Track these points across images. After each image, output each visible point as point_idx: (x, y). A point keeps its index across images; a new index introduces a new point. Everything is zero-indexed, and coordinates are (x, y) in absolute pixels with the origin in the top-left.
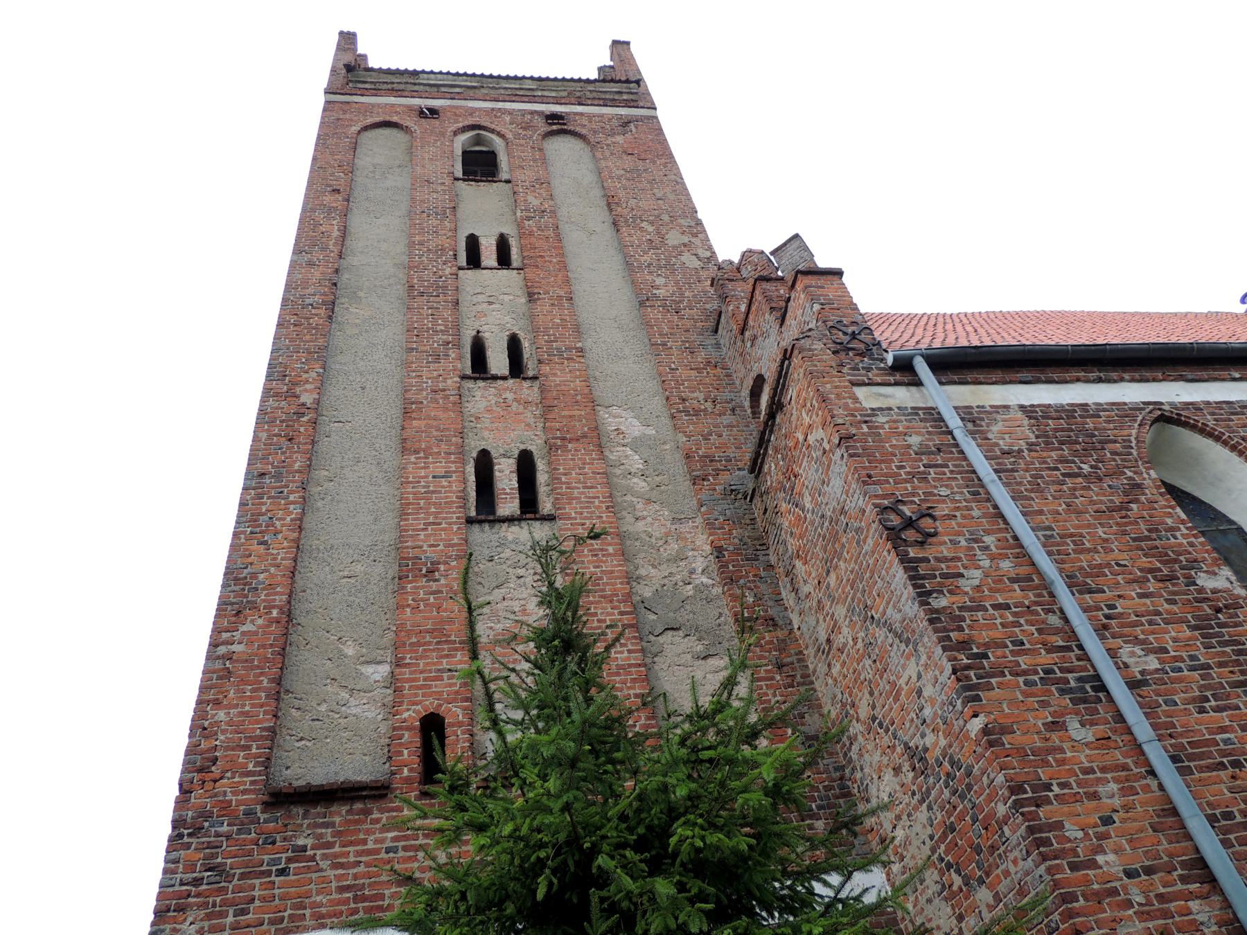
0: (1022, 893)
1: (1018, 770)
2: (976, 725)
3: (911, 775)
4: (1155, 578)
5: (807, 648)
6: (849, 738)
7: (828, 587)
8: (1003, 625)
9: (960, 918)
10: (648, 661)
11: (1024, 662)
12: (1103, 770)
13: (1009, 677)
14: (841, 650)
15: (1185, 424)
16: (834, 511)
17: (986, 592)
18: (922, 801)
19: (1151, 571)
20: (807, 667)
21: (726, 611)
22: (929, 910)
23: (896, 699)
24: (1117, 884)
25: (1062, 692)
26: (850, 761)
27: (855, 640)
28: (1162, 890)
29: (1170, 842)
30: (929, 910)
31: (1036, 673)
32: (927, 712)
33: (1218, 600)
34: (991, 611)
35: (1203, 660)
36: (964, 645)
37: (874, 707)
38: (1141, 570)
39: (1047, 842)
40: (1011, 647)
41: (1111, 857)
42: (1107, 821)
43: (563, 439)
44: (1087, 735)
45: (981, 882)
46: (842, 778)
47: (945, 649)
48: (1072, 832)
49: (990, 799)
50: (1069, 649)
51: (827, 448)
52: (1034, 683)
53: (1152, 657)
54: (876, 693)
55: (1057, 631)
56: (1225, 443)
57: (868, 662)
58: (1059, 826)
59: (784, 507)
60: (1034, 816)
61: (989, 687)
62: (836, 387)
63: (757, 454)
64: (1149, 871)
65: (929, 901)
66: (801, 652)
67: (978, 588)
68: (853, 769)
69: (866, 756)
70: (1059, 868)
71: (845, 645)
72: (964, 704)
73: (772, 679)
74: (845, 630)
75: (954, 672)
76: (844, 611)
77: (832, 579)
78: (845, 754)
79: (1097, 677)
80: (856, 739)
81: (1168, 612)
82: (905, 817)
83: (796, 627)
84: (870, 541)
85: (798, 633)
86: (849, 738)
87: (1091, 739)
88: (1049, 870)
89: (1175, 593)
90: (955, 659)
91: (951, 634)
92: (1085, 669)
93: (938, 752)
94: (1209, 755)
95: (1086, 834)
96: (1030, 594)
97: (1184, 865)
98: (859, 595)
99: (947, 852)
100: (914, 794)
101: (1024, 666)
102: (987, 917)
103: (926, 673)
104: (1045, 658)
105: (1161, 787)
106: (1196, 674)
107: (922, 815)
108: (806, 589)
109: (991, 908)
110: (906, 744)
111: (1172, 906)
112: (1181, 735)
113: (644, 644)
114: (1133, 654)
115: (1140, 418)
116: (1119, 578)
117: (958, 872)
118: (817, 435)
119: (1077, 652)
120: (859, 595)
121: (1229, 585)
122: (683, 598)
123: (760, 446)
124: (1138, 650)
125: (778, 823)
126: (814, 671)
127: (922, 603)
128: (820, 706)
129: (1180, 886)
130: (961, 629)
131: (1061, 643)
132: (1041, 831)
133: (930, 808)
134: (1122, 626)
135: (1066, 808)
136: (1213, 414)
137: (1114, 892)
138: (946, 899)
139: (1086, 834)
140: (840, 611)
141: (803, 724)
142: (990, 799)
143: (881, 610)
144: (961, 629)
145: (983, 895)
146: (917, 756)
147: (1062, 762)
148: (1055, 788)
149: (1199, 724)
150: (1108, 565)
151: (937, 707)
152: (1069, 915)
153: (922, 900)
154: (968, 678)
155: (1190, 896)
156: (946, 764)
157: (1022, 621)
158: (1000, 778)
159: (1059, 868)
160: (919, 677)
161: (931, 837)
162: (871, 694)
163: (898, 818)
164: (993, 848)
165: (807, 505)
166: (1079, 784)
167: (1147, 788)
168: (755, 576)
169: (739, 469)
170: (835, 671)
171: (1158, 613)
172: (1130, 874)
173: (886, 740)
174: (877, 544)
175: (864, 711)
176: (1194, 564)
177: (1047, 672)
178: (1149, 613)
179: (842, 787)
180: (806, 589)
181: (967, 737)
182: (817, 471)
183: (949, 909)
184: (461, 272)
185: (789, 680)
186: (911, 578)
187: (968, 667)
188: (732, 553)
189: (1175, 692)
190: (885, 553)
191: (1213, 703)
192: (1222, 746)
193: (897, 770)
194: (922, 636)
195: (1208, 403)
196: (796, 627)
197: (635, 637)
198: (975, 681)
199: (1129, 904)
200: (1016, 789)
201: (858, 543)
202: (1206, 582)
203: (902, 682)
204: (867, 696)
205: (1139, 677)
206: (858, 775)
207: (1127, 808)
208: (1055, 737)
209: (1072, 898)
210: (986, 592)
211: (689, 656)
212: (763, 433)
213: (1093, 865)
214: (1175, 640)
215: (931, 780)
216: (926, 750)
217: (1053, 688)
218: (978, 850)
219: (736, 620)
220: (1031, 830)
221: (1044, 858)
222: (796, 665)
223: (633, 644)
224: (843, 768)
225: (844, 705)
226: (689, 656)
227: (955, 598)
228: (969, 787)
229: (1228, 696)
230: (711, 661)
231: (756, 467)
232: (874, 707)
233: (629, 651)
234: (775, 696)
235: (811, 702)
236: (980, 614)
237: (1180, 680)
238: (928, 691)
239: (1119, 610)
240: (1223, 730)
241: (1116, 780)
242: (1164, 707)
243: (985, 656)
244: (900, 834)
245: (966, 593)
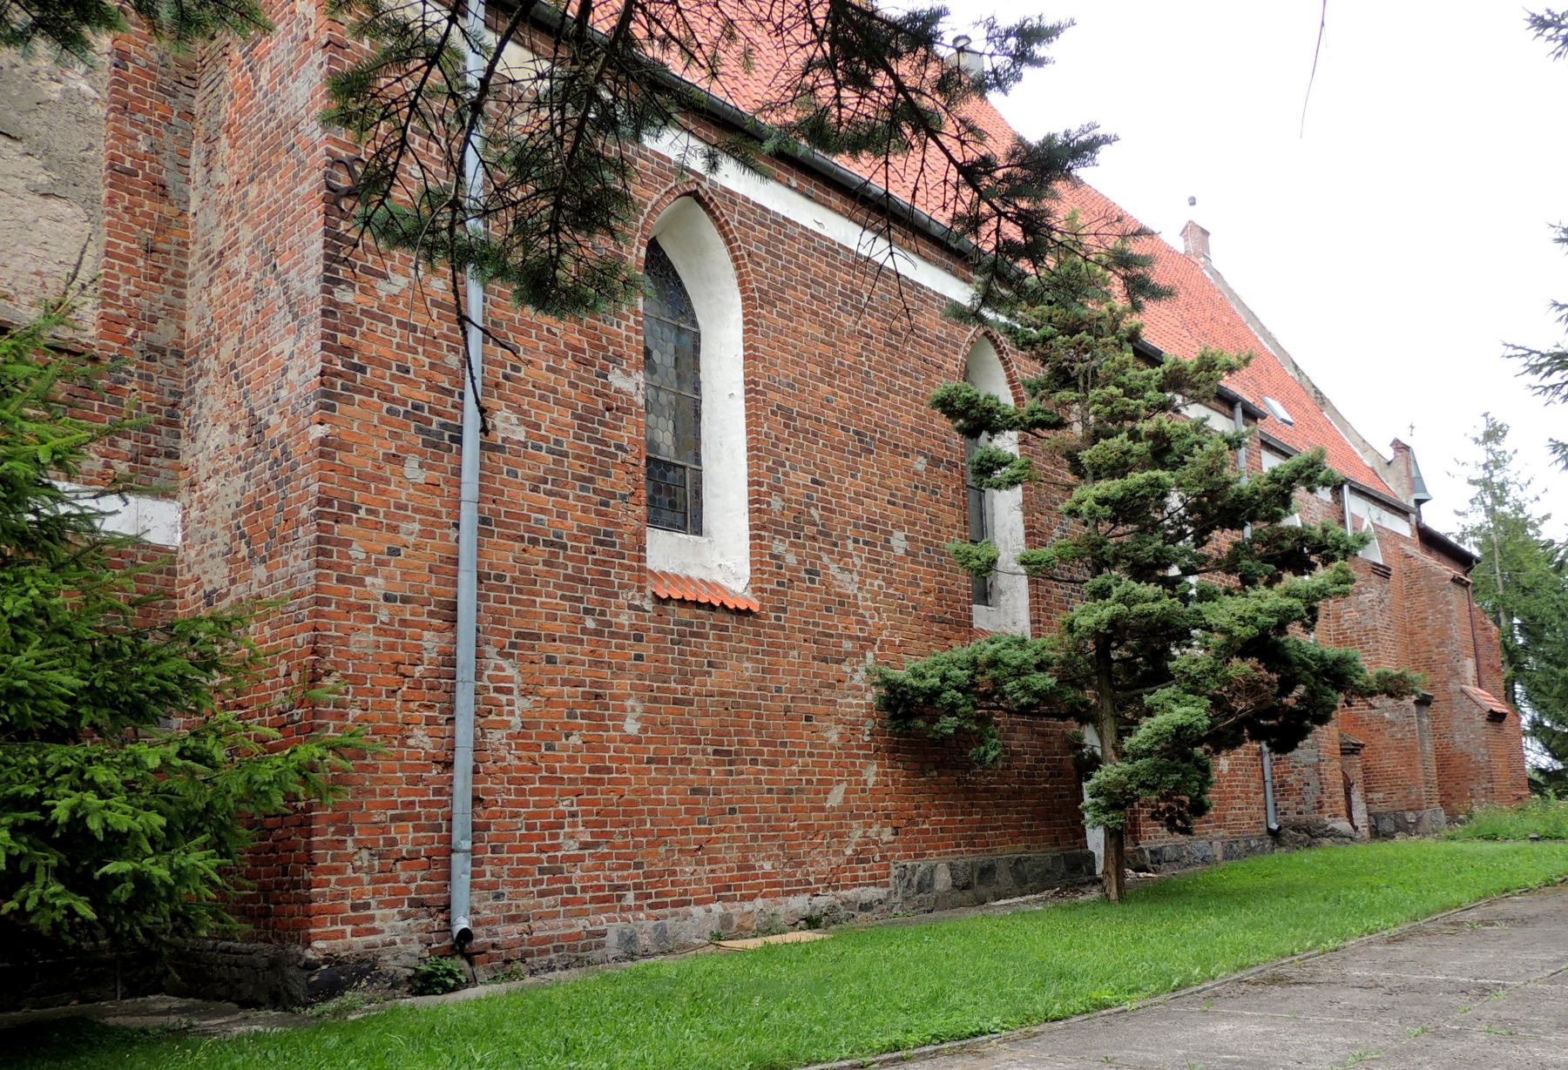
0: (290, 584)
1: (335, 484)
2: (318, 432)
3: (244, 440)
4: (574, 357)
5: (195, 243)
6: (201, 369)
7: (246, 195)
8: (399, 346)
9: (233, 582)
11: (399, 390)
13: (375, 399)
15: (711, 212)
16: (287, 117)
17: (401, 306)
18: (243, 469)
19: (575, 349)
20: (186, 265)
21: (101, 145)
22: (209, 564)
23: (262, 362)
24: (372, 603)
25: (419, 430)
26: (192, 392)
28: (408, 617)
29: (438, 584)
30: (209, 564)
31: (405, 404)
32: (283, 393)
33: (615, 400)
34: (394, 327)
35: (565, 448)
36: (346, 351)
37: (237, 356)
38: (566, 345)
39: (329, 554)
40: (394, 370)
41: (379, 581)
42: (394, 552)
44: (420, 476)
45: (263, 560)
46: (174, 405)
47: (324, 347)
48: (356, 551)
49: (299, 499)
50: (450, 393)
51: (312, 37)
52: (397, 413)
53: (522, 429)
54: (246, 343)
55: (450, 372)
56: (732, 250)
57: (251, 308)
58: (348, 544)
59: (236, 54)
60: (329, 529)
61: (350, 401)
64: (405, 600)
65: (213, 556)
66: (185, 244)
67: (394, 298)
69: (210, 398)
71: (236, 272)
74: (243, 258)
75: (322, 374)
76: (250, 237)
77: (253, 190)
78: (190, 383)
79: (460, 429)
80: (207, 374)
81: (564, 394)
82: (222, 474)
83: (192, 210)
84: (306, 184)
85: (191, 219)
86: (201, 369)
88: (317, 576)
89: (581, 379)
90: (330, 362)
91: (339, 335)
92: (454, 417)
93: (276, 435)
94: (516, 527)
95: (368, 558)
96: (445, 325)
97: (438, 603)
98: (272, 232)
99: (246, 523)
100: (239, 458)
101: (396, 394)
102: (255, 590)
103: (298, 356)
104: (422, 394)
105: (457, 540)
106: (551, 457)
109: (261, 584)
110: (252, 410)
111: (409, 631)
112: (504, 504)
115: (672, 185)
116: (541, 344)
117: (248, 544)
119: (456, 399)
120: (272, 232)
121: (633, 390)
122: (41, 98)
124: (514, 418)
126: (192, 275)
127: (326, 290)
128: (183, 317)
129: (425, 618)
130: (352, 333)
132: (328, 543)
133: (247, 479)
134: (514, 390)
135: (362, 531)
136: (742, 214)
137: (366, 608)
138: (228, 561)
140: (247, 234)
141: (151, 330)
142: (299, 499)
143: (286, 265)
144: (352, 333)
145: (260, 572)
146: (257, 428)
147: (380, 492)
149: (523, 499)
150: (539, 327)
151: (293, 395)
152: (317, 614)
153: (207, 553)
154: (333, 385)
155: (429, 627)
156: (278, 449)
157: (420, 349)
158: (315, 488)
159: (327, 577)
161: (238, 505)
162: (241, 341)
163: (216, 471)
165: (263, 82)
166: (386, 515)
167: (445, 537)
168: (163, 117)
170: (216, 290)
171: (554, 391)
172: (387, 598)
174: (310, 196)
175: (226, 353)
176: (617, 359)
177: (415, 407)
178: (547, 388)
179: (171, 415)
180: (220, 177)
181: (305, 438)
182: (290, 52)
183: (226, 571)
185: (155, 272)
186: (327, 257)
187: (338, 375)
188: (139, 70)
189: (522, 466)
190: (315, 212)
191: (549, 486)
192: (532, 524)
193: (234, 428)
194: (310, 321)
195: (747, 200)
196: (192, 210)
198: (339, 390)
199: (373, 620)
200: (324, 501)
201: (295, 176)
202: (617, 379)
205: (500, 442)
207: (417, 547)
208: (388, 469)
210: (401, 306)
211: (22, 184)
213: (360, 582)
214: (553, 421)
215: (260, 456)
217: (413, 424)
219: (111, 166)
220: (319, 540)
221: (319, 565)
222: (172, 256)
224: (181, 395)
225: (209, 333)
226: (22, 184)
227: (363, 298)
228: (288, 480)
229: (565, 485)
230: (53, 204)
232: (237, 356)
235: (175, 313)
236: (381, 325)
237: (533, 457)
239: (522, 375)
240: (542, 511)
241: (422, 522)
242: (505, 476)
243: (362, 370)
244: (211, 486)
245: (379, 298)
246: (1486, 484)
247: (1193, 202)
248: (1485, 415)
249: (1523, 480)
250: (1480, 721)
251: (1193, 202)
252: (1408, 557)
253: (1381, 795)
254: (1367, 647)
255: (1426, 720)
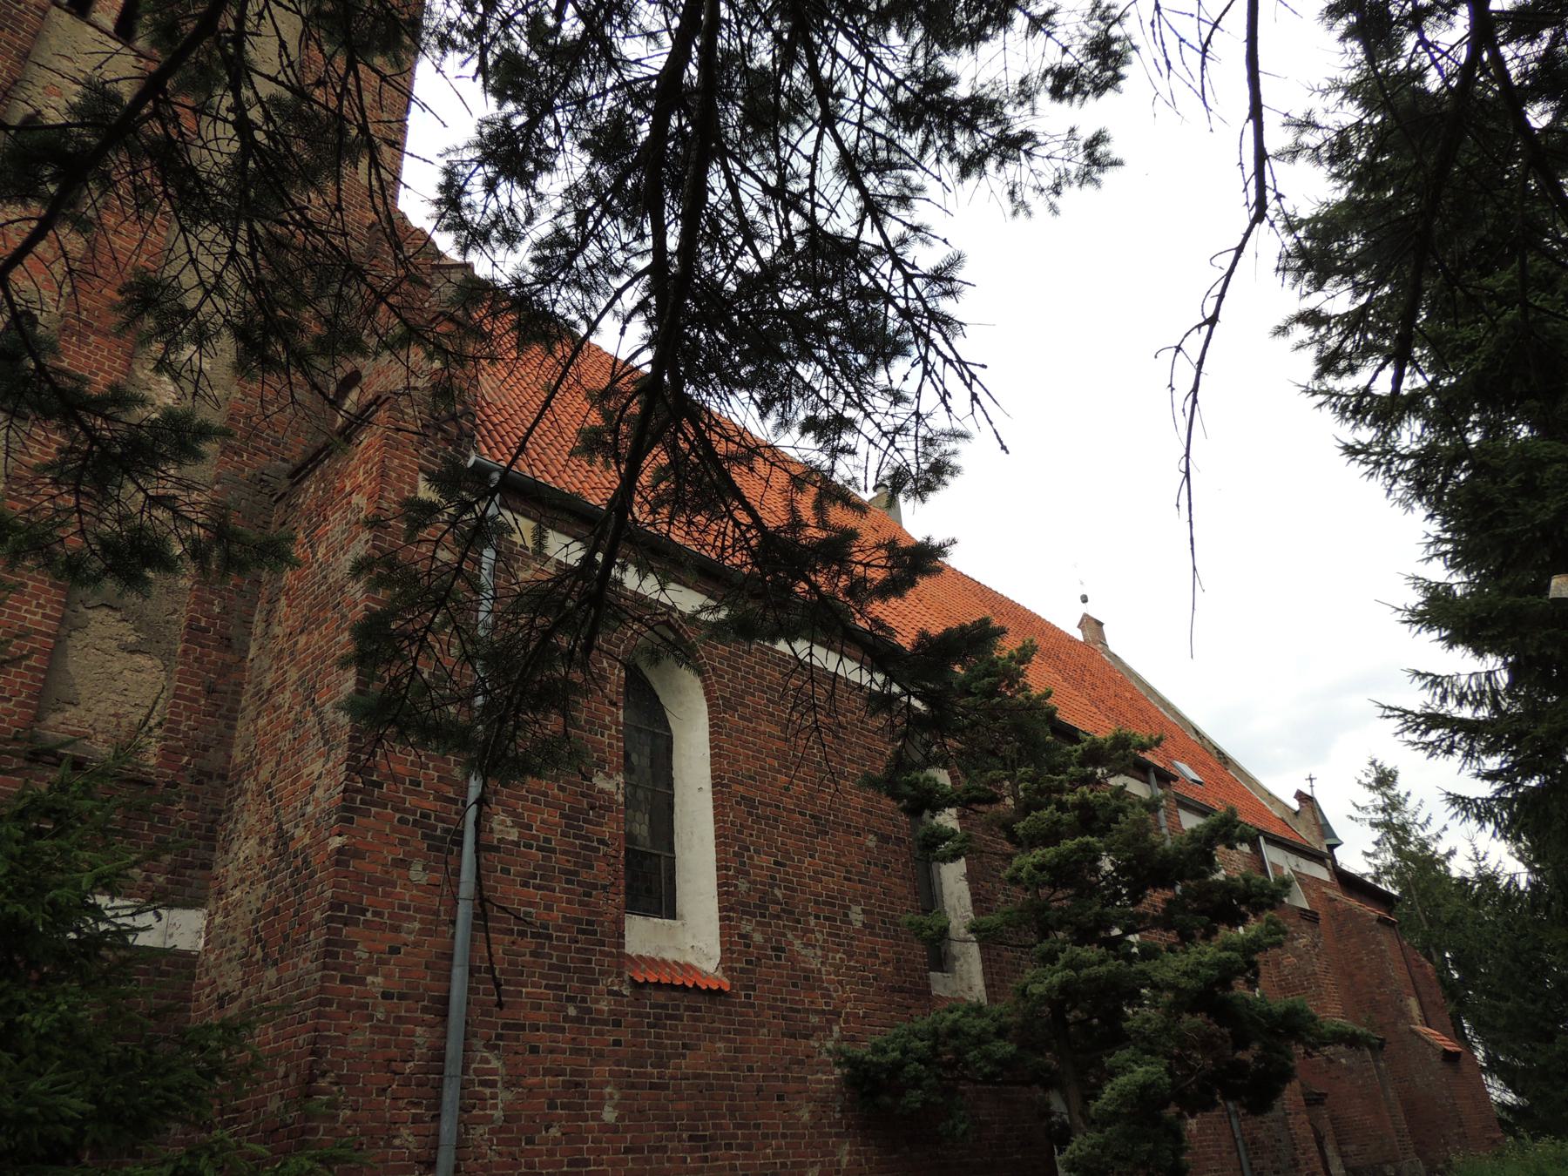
0: (297, 986)
2: (336, 842)
3: (271, 851)
7: (296, 643)
9: (245, 984)
10: (64, 632)
12: (417, 910)
14: (276, 708)
18: (267, 878)
21: (184, 611)
22: (226, 967)
23: (294, 782)
24: (370, 1001)
27: (291, 708)
30: (226, 967)
32: (309, 809)
37: (273, 777)
43: (88, 325)
45: (275, 963)
46: (213, 822)
49: (314, 905)
52: (406, 822)
60: (338, 932)
61: (367, 814)
62: (404, 466)
63: (304, 466)
64: (402, 997)
66: (241, 684)
68: (229, 819)
70: (333, 978)
71: (281, 706)
72: (337, 822)
73: (196, 701)
74: (288, 694)
76: (295, 677)
77: (302, 640)
78: (230, 801)
81: (554, 797)
87: (424, 882)
90: (353, 780)
93: (299, 846)
95: (371, 957)
97: (432, 999)
102: (265, 991)
104: (430, 804)
105: (453, 937)
106: (540, 854)
107: (261, 889)
108: (277, 630)
109: (271, 987)
111: (403, 1027)
113: (69, 613)
114: (503, 823)
117: (263, 948)
118: (358, 499)
123: (311, 460)
125: (848, 63)
126: (244, 709)
129: (418, 1014)
131: (451, 795)
133: (269, 887)
138: (242, 965)
139: (371, 957)
140: (293, 675)
142: (314, 905)
145: (271, 974)
146: (283, 838)
147: (386, 894)
148: (369, 915)
153: (225, 956)
154: (353, 800)
155: (422, 1023)
158: (329, 894)
160: (319, 777)
161: (259, 911)
162: (278, 764)
163: (242, 881)
164: (297, 942)
165: (319, 555)
169: (283, 460)
170: (262, 722)
173: (268, 811)
176: (600, 764)
177: (423, 816)
179: (210, 830)
180: (277, 630)
184: (54, 10)
185: (212, 709)
187: (358, 791)
193: (263, 841)
197: (59, 602)
199: (371, 1018)
200: (336, 906)
202: (600, 782)
203: (306, 771)
204: (273, 764)
206: (231, 826)
207: (416, 945)
209: (329, 1003)
211: (115, 643)
212: (320, 452)
213: (361, 981)
216: (292, 838)
218: (286, 938)
220: (328, 942)
223: (53, 609)
225: (251, 757)
226: (115, 643)
228: (306, 887)
231: (298, 474)
232: (273, 777)
233: (44, 616)
234: (189, 719)
235: (225, 742)
237: (524, 855)
238: (319, 793)
240: (531, 904)
241: (422, 921)
244: (237, 893)
246: (1387, 826)
247: (1085, 599)
248: (1373, 763)
249: (1421, 819)
250: (1436, 1061)
251: (1085, 599)
252: (1332, 900)
253: (1354, 1147)
254: (1310, 992)
255: (1382, 1065)
